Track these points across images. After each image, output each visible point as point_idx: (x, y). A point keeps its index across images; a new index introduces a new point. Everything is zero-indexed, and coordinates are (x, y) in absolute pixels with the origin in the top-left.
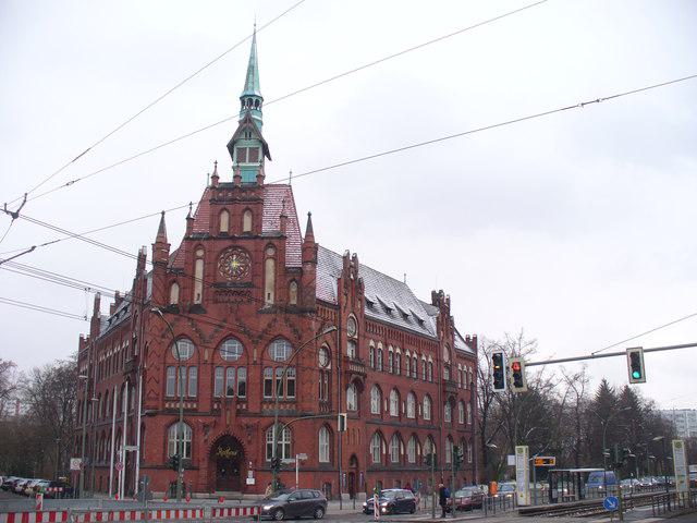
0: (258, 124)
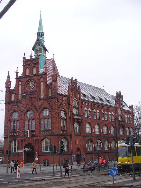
0: (42, 41)
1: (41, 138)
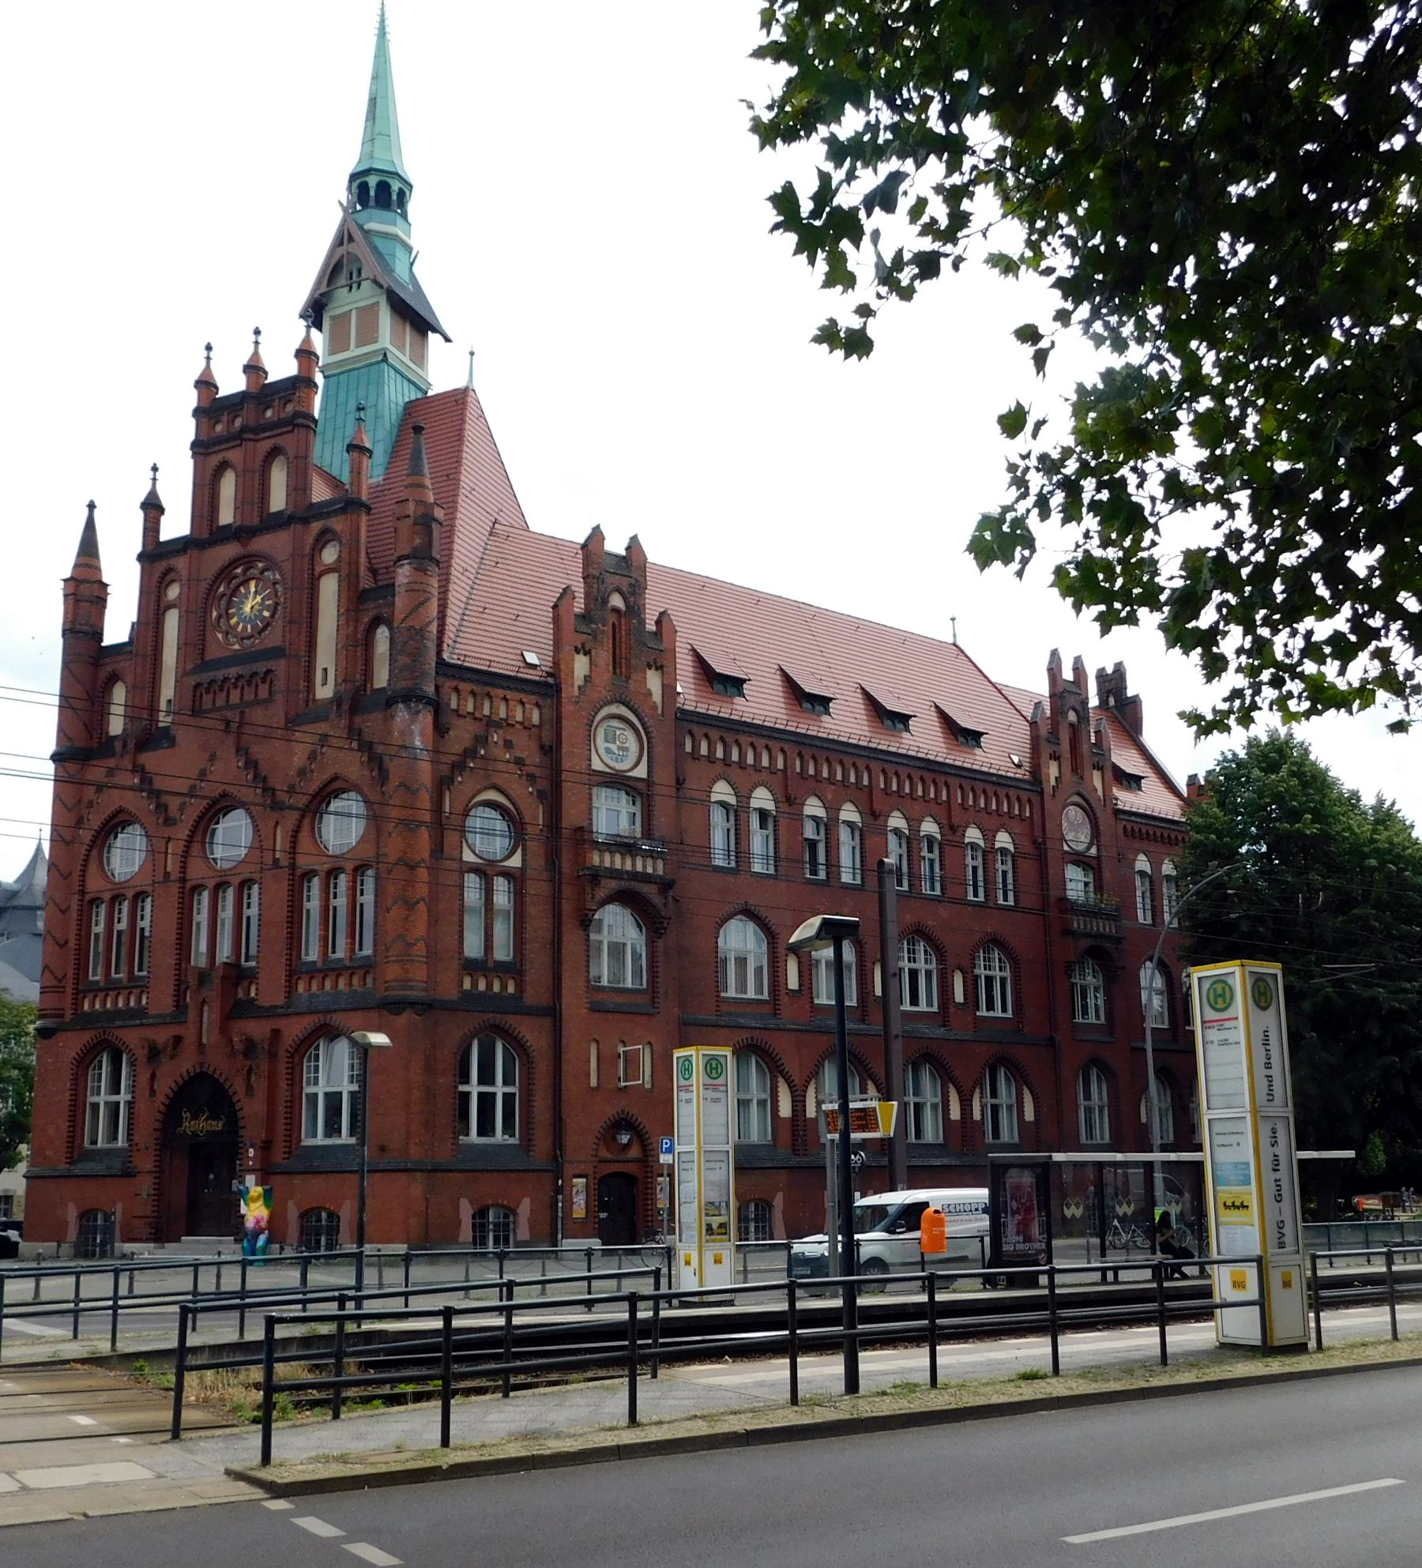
1: (294, 1029)
